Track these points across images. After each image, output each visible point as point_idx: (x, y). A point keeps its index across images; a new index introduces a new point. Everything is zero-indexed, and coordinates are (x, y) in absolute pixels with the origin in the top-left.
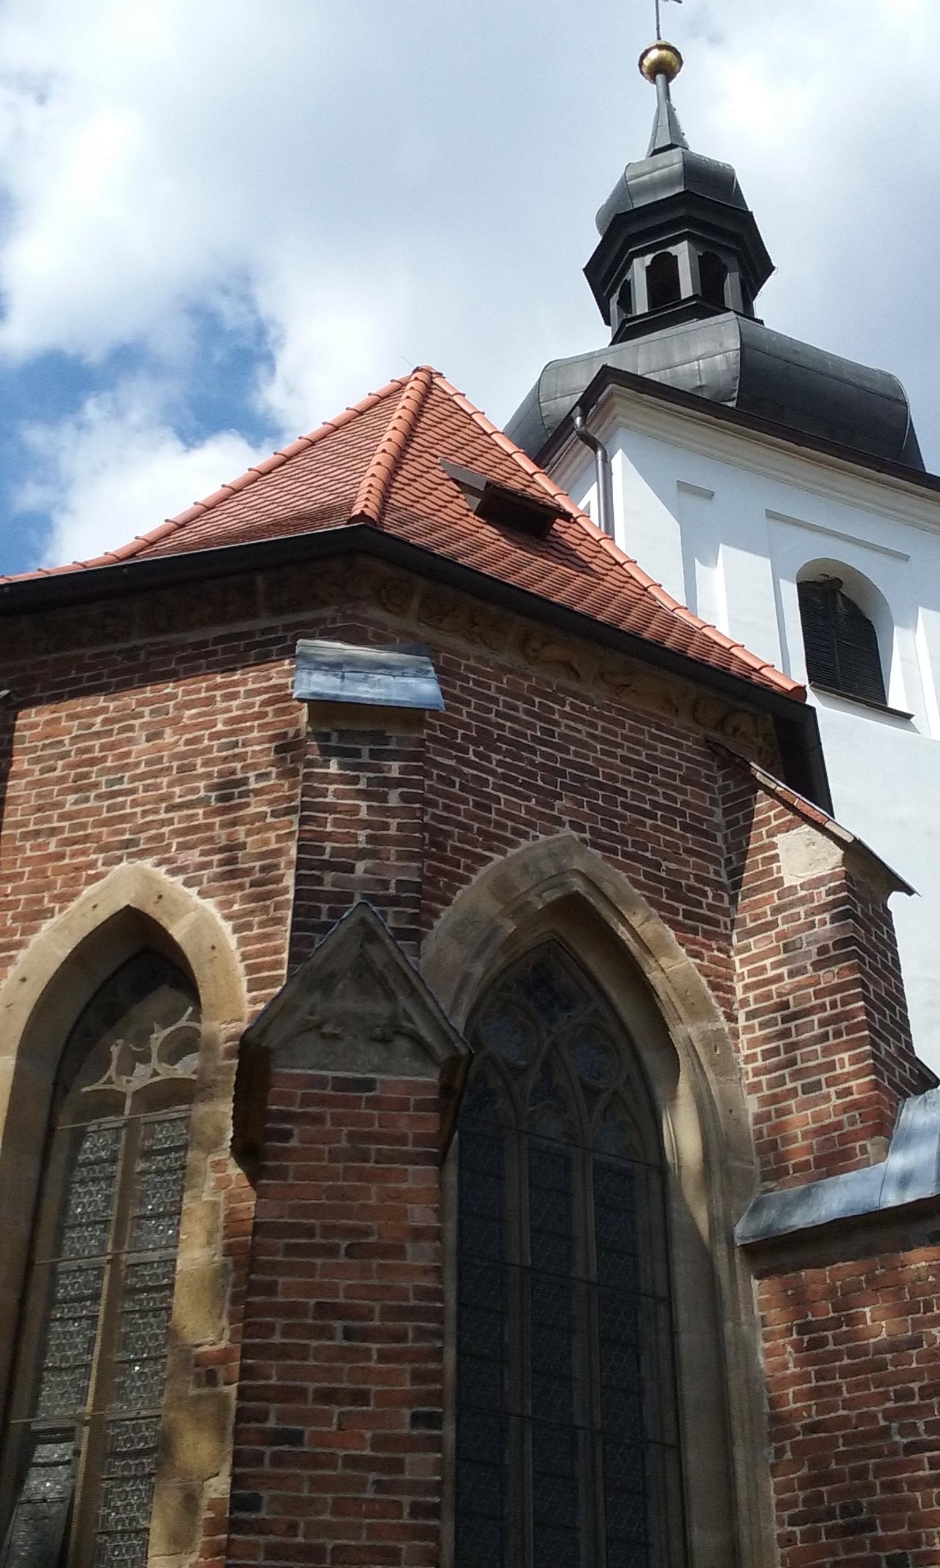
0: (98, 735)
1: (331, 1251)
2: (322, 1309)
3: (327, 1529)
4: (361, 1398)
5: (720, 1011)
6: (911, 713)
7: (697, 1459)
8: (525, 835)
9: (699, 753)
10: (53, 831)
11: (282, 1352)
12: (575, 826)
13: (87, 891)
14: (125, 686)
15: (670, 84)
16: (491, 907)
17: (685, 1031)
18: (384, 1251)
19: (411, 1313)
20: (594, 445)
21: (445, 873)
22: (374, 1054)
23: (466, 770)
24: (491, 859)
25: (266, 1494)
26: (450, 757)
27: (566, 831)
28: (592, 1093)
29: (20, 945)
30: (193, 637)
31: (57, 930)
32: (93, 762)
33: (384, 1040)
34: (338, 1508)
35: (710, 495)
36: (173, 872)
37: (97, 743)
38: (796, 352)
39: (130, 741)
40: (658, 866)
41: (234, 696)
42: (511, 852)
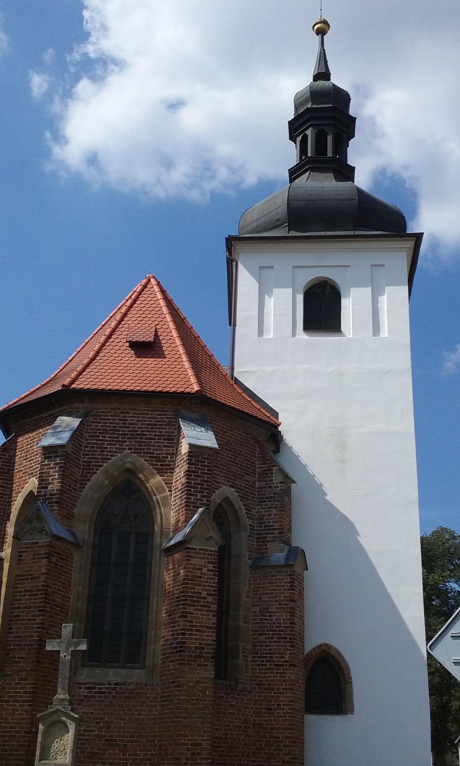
1: (27, 579)
4: (30, 607)
5: (167, 490)
8: (114, 456)
9: (172, 415)
11: (18, 600)
12: (129, 449)
14: (34, 430)
15: (324, 37)
18: (36, 578)
21: (89, 473)
23: (99, 442)
24: (103, 465)
25: (14, 627)
26: (94, 440)
29: (109, 459)
38: (311, 195)
40: (153, 453)
42: (109, 461)
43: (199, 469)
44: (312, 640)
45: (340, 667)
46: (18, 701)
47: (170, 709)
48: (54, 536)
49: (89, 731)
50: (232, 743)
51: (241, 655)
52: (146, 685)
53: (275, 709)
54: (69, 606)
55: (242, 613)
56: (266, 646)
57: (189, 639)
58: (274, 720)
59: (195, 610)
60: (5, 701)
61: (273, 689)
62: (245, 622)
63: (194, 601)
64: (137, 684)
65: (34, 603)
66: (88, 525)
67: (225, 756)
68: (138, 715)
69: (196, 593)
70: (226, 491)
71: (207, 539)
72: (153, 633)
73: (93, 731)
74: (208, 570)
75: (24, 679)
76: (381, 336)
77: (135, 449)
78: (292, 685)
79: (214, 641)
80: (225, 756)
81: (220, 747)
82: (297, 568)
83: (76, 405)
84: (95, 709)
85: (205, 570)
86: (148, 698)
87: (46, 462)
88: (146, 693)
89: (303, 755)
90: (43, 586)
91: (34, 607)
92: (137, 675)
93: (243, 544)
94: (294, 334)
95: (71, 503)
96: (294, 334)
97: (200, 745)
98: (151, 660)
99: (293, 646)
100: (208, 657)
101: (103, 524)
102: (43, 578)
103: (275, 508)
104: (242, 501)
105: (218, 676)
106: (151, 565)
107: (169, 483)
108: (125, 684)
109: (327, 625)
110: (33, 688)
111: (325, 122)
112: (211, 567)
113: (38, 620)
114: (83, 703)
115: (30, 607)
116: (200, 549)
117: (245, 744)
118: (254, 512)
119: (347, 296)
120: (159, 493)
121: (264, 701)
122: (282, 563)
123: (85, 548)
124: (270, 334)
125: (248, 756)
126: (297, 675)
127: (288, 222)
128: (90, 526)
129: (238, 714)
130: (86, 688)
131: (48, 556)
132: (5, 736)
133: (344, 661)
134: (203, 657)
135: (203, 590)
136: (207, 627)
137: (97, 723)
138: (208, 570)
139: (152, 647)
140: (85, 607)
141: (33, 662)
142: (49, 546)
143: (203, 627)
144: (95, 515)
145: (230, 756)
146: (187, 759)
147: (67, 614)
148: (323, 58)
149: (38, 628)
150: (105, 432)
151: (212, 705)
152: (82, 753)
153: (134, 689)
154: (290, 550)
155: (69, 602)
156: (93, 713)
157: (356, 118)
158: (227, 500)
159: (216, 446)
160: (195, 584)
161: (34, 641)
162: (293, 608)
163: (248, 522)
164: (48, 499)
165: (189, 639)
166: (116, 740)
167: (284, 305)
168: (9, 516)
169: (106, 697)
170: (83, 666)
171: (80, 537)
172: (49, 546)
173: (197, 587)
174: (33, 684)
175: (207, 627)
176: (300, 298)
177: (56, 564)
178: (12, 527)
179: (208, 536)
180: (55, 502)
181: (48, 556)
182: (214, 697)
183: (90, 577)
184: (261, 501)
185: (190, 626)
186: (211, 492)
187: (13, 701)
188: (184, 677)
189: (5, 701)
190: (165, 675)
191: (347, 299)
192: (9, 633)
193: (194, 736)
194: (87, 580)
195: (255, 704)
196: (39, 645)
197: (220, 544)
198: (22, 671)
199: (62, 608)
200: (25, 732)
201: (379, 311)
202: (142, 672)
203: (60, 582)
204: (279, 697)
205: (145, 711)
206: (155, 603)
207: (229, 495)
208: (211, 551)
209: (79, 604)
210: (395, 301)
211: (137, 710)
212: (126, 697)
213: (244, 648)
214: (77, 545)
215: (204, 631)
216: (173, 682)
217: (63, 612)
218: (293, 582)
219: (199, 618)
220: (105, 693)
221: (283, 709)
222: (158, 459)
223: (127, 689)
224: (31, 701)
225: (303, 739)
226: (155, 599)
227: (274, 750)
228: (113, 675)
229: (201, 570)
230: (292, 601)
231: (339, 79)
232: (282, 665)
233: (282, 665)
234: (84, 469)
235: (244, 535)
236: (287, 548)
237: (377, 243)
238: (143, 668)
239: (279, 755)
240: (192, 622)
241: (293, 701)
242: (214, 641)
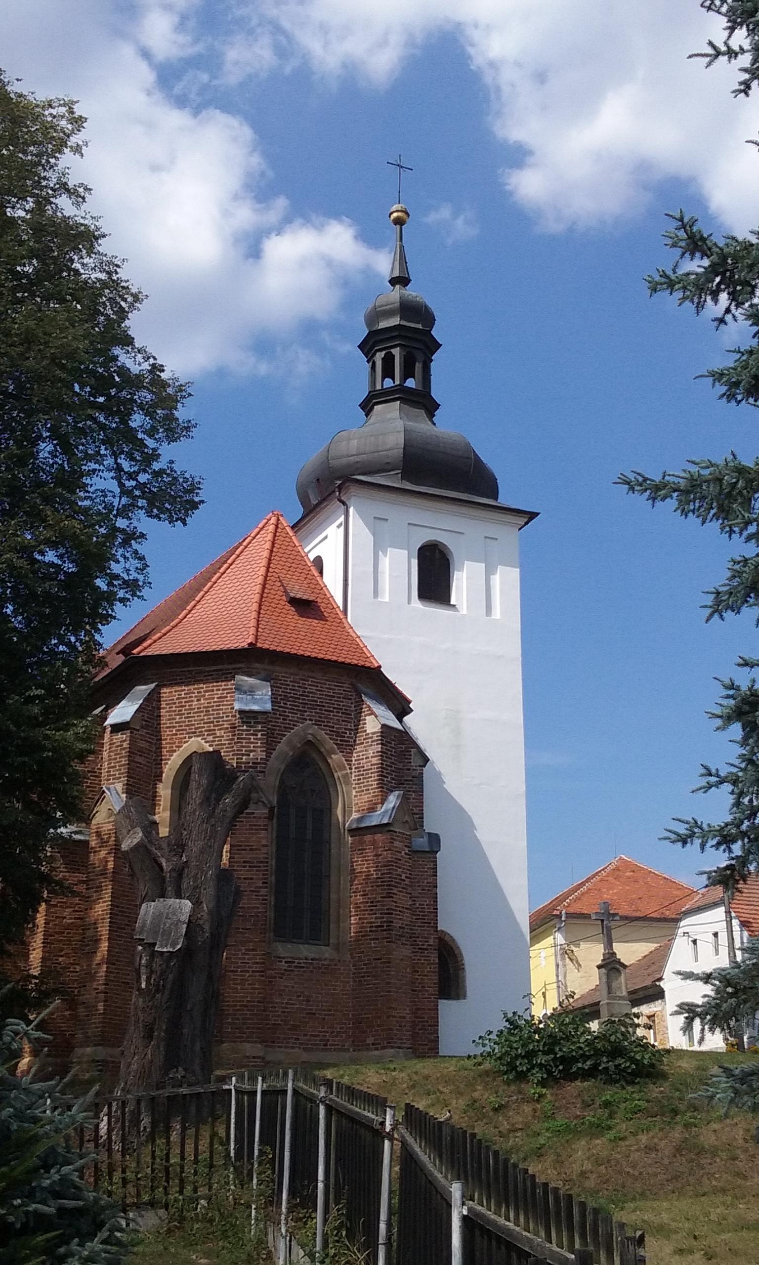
0: (183, 698)
1: (245, 850)
2: (244, 862)
4: (252, 879)
6: (739, 72)
7: (333, 878)
10: (174, 727)
12: (310, 720)
13: (185, 745)
16: (286, 749)
17: (338, 774)
18: (256, 849)
19: (261, 862)
20: (344, 503)
27: (308, 722)
28: (313, 791)
29: (169, 759)
30: (207, 669)
31: (179, 756)
32: (183, 706)
36: (206, 742)
37: (183, 701)
39: (192, 701)
41: (218, 690)
45: (455, 956)
53: (420, 991)
64: (331, 960)
68: (334, 989)
75: (253, 950)
76: (493, 617)
77: (316, 721)
83: (257, 665)
84: (296, 983)
86: (342, 974)
87: (245, 727)
88: (339, 969)
92: (327, 952)
94: (409, 602)
96: (409, 602)
103: (414, 792)
107: (349, 761)
108: (320, 960)
114: (284, 977)
119: (461, 569)
120: (341, 770)
124: (386, 597)
127: (403, 470)
130: (286, 962)
157: (439, 346)
166: (314, 1014)
167: (399, 568)
168: (161, 776)
175: (407, 909)
176: (415, 562)
178: (167, 788)
191: (460, 573)
201: (490, 587)
210: (506, 582)
221: (427, 991)
232: (426, 949)
233: (426, 949)
237: (504, 516)
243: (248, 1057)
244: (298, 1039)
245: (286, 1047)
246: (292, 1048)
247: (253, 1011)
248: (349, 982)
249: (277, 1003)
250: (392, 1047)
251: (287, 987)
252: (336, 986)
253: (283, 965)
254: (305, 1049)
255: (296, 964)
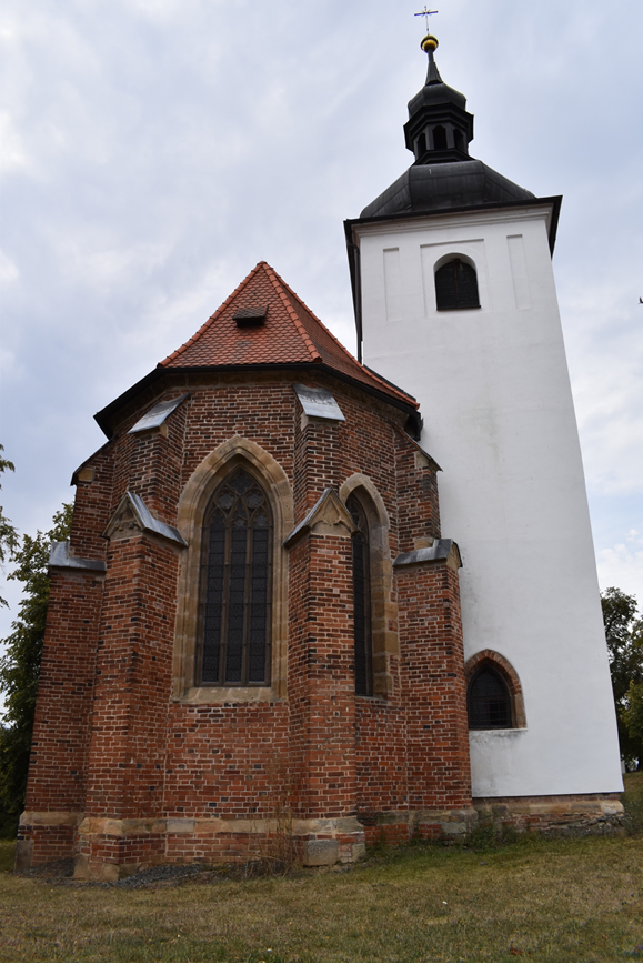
1: (118, 584)
3: (115, 646)
4: (122, 616)
5: (286, 475)
11: (109, 609)
12: (239, 432)
22: (130, 532)
29: (216, 445)
33: (131, 528)
34: (117, 641)
35: (397, 249)
43: (323, 445)
44: (473, 646)
46: (112, 728)
47: (302, 732)
48: (148, 531)
49: (204, 761)
50: (383, 769)
51: (389, 667)
52: (272, 705)
53: (433, 727)
54: (174, 616)
55: (387, 619)
56: (419, 654)
57: (320, 646)
58: (433, 740)
59: (325, 610)
60: (98, 729)
61: (430, 704)
62: (391, 629)
63: (324, 600)
64: (261, 704)
65: (127, 611)
66: (193, 521)
67: (376, 784)
69: (326, 590)
70: (358, 478)
71: (336, 525)
72: (278, 643)
73: (209, 761)
74: (340, 562)
75: (118, 702)
78: (453, 697)
79: (352, 647)
80: (376, 784)
81: (370, 774)
82: (451, 563)
83: (175, 388)
84: (210, 736)
85: (335, 562)
86: (276, 720)
89: (470, 778)
90: (135, 590)
91: (127, 616)
92: (261, 694)
93: (383, 539)
95: (172, 497)
97: (342, 774)
98: (277, 675)
99: (451, 653)
100: (345, 667)
101: (213, 520)
102: (135, 581)
103: (419, 497)
104: (379, 491)
105: (361, 688)
106: (272, 565)
108: (246, 704)
109: (491, 627)
110: (128, 712)
111: (438, 120)
112: (343, 558)
113: (132, 630)
115: (122, 616)
116: (328, 537)
117: (399, 769)
118: (394, 504)
121: (419, 718)
122: (432, 558)
123: (191, 549)
125: (404, 783)
126: (459, 685)
128: (196, 524)
129: (389, 735)
130: (199, 711)
131: (142, 555)
132: (99, 771)
133: (512, 667)
134: (339, 667)
135: (334, 586)
136: (342, 631)
137: (215, 752)
138: (340, 562)
139: (278, 660)
140: (195, 617)
141: (127, 681)
142: (142, 543)
143: (337, 630)
144: (203, 511)
145: (381, 784)
146: (325, 792)
147: (172, 625)
148: (433, 69)
149: (131, 640)
150: (210, 415)
151: (354, 725)
152: (197, 788)
153: (257, 710)
154: (440, 543)
155: (175, 611)
156: (208, 741)
158: (361, 489)
159: (343, 418)
160: (324, 580)
161: (127, 656)
162: (448, 608)
163: (389, 515)
164: (142, 491)
165: (320, 646)
169: (224, 721)
170: (196, 686)
171: (184, 536)
172: (142, 543)
173: (326, 583)
174: (128, 707)
175: (342, 631)
177: (153, 565)
179: (337, 521)
180: (150, 494)
181: (142, 555)
182: (357, 716)
183: (200, 582)
184: (402, 491)
185: (320, 630)
186: (339, 478)
187: (107, 729)
188: (316, 693)
189: (98, 729)
190: (294, 692)
192: (100, 648)
193: (333, 764)
194: (197, 586)
195: (408, 722)
196: (133, 660)
197: (352, 530)
198: (114, 692)
199: (165, 617)
200: (121, 766)
202: (268, 690)
203: (160, 587)
204: (438, 712)
205: (272, 735)
206: (278, 608)
207: (363, 483)
208: (342, 539)
209: (187, 614)
211: (263, 735)
212: (248, 720)
213: (392, 659)
214: (181, 547)
215: (340, 636)
216: (303, 700)
217: (167, 623)
218: (446, 579)
219: (331, 620)
220: (222, 716)
221: (443, 726)
222: (274, 441)
223: (249, 710)
224: (124, 728)
225: (469, 760)
226: (278, 603)
227: (435, 774)
228: (232, 695)
229: (331, 562)
230: (447, 600)
231: (450, 79)
233: (440, 676)
234: (186, 459)
235: (385, 529)
236: (435, 543)
238: (269, 685)
239: (441, 779)
240: (323, 625)
241: (455, 716)
242: (352, 647)
243: (103, 836)
244: (214, 805)
245: (197, 815)
246: (208, 816)
247: (115, 777)
248: (286, 729)
249: (186, 762)
250: (317, 816)
251: (201, 741)
252: (267, 735)
253: (196, 715)
254: (224, 817)
255: (212, 713)
